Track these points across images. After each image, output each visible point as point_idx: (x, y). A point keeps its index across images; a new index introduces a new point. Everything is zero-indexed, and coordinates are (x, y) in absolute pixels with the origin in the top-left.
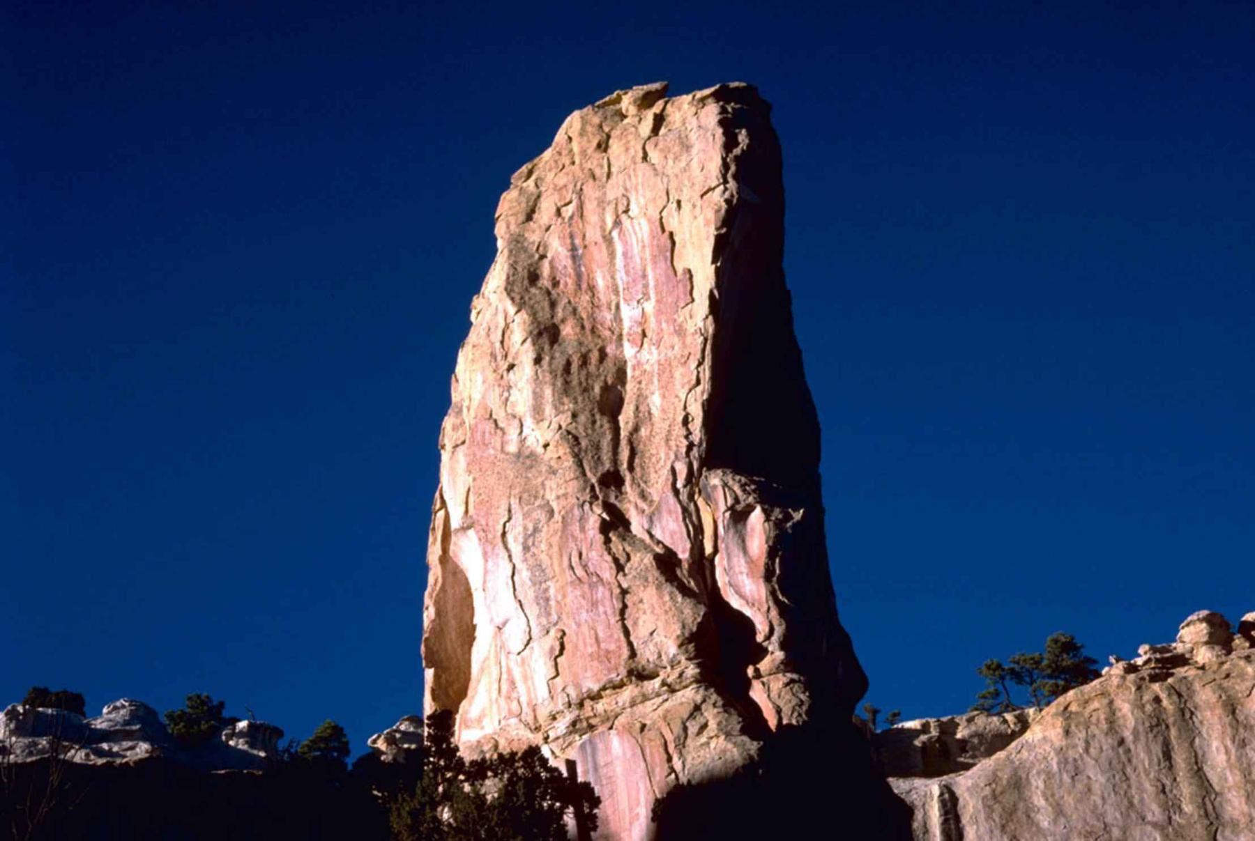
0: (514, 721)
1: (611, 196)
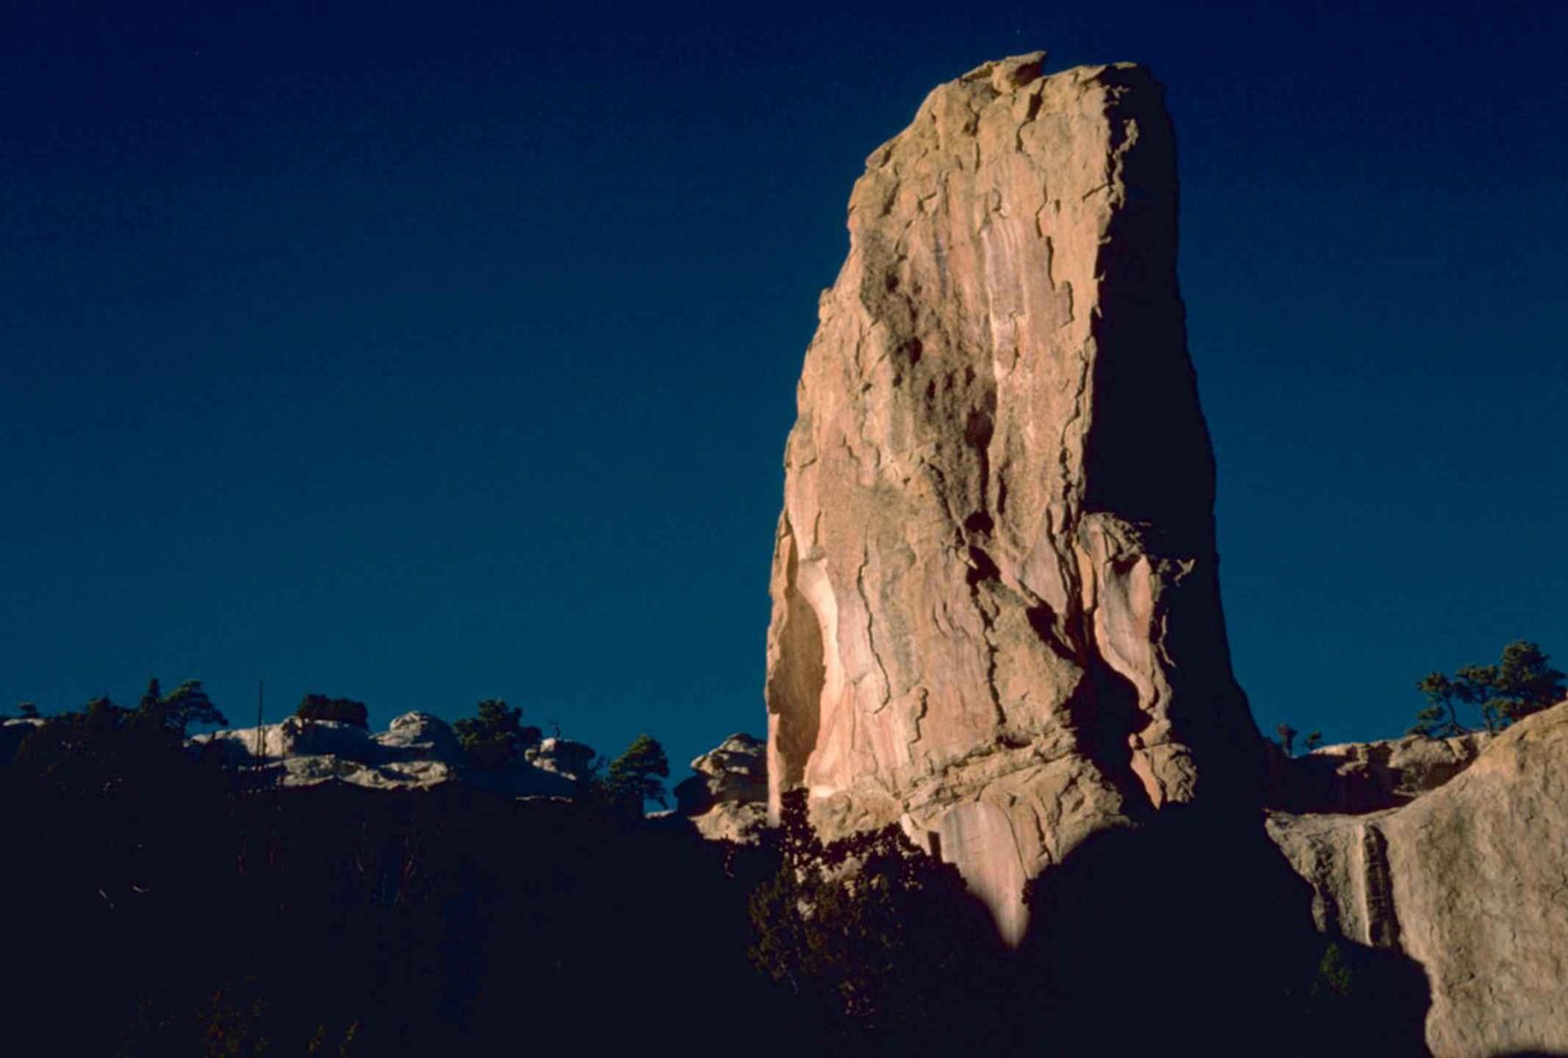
0: (868, 779)
1: (980, 189)
